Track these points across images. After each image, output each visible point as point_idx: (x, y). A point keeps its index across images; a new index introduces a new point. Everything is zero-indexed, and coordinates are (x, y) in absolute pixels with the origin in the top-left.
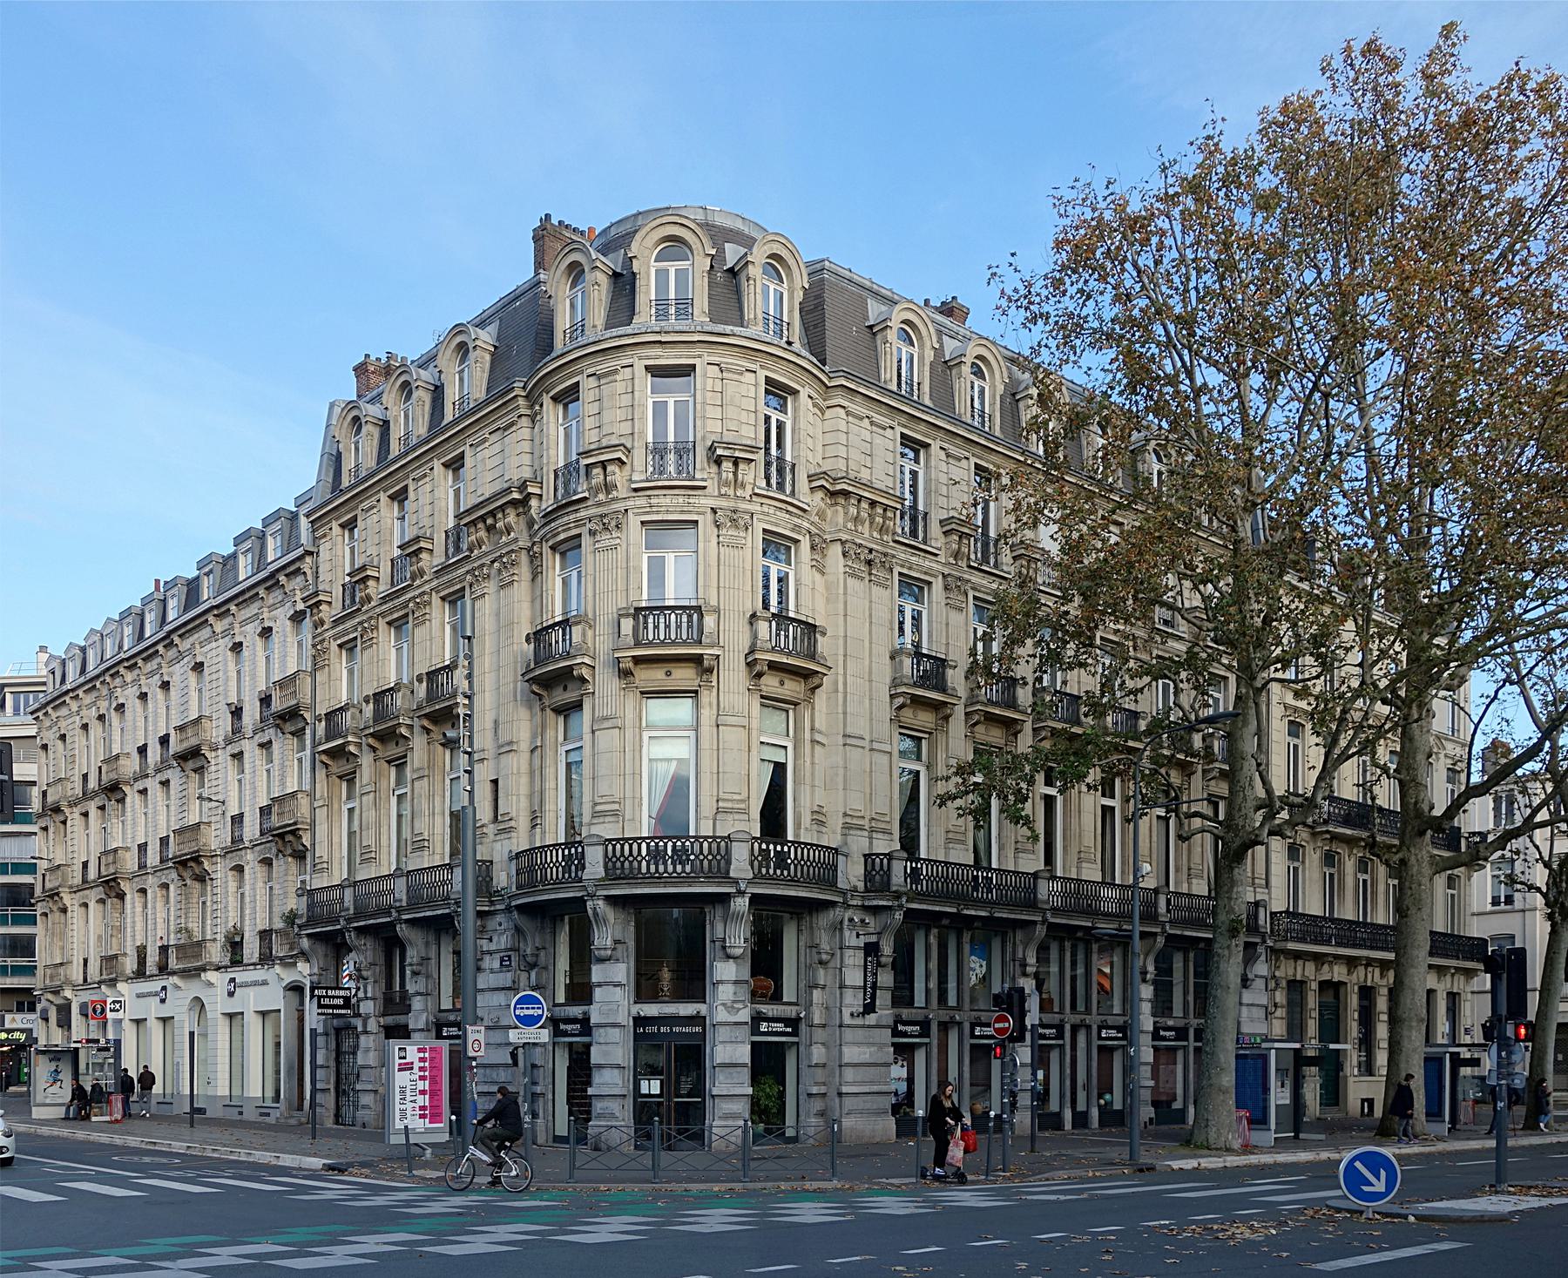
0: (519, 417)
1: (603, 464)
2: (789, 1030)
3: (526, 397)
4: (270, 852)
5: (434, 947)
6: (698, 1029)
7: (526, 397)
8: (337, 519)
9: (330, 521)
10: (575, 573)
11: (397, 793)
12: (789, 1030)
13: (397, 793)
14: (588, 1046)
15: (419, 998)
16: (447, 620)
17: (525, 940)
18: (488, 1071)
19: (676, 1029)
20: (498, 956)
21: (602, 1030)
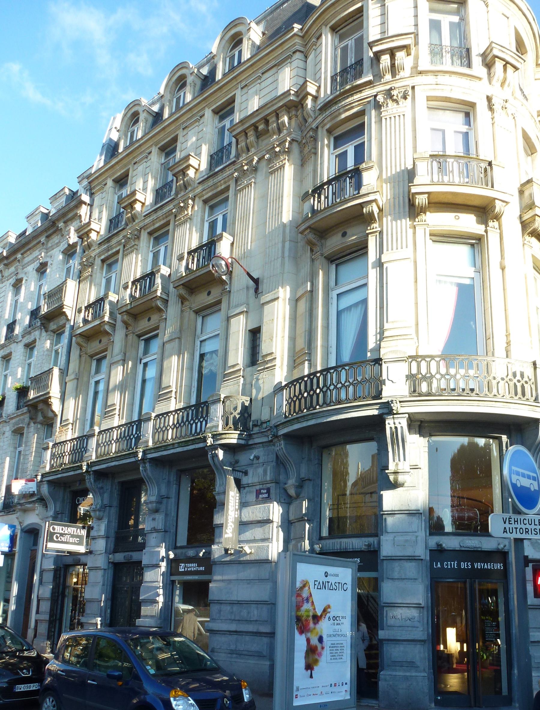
0: (294, 53)
1: (392, 52)
2: (202, 569)
3: (303, 37)
4: (22, 423)
5: (174, 487)
6: (499, 566)
7: (303, 37)
8: (208, 106)
9: (106, 179)
10: (162, 249)
11: (144, 361)
12: (202, 569)
13: (144, 361)
14: (208, 582)
15: (154, 535)
16: (206, 218)
17: (287, 473)
18: (235, 608)
19: (478, 565)
20: (254, 489)
21: (396, 564)
